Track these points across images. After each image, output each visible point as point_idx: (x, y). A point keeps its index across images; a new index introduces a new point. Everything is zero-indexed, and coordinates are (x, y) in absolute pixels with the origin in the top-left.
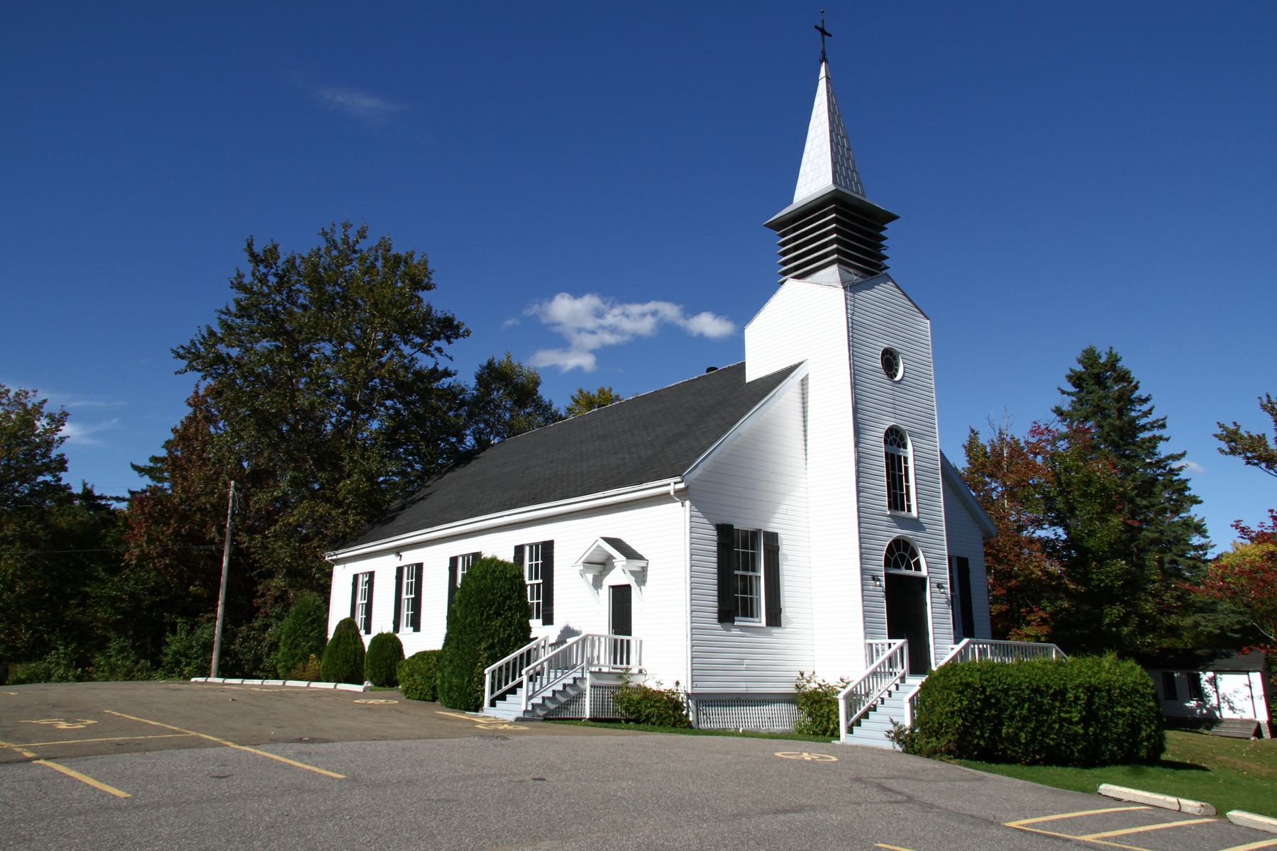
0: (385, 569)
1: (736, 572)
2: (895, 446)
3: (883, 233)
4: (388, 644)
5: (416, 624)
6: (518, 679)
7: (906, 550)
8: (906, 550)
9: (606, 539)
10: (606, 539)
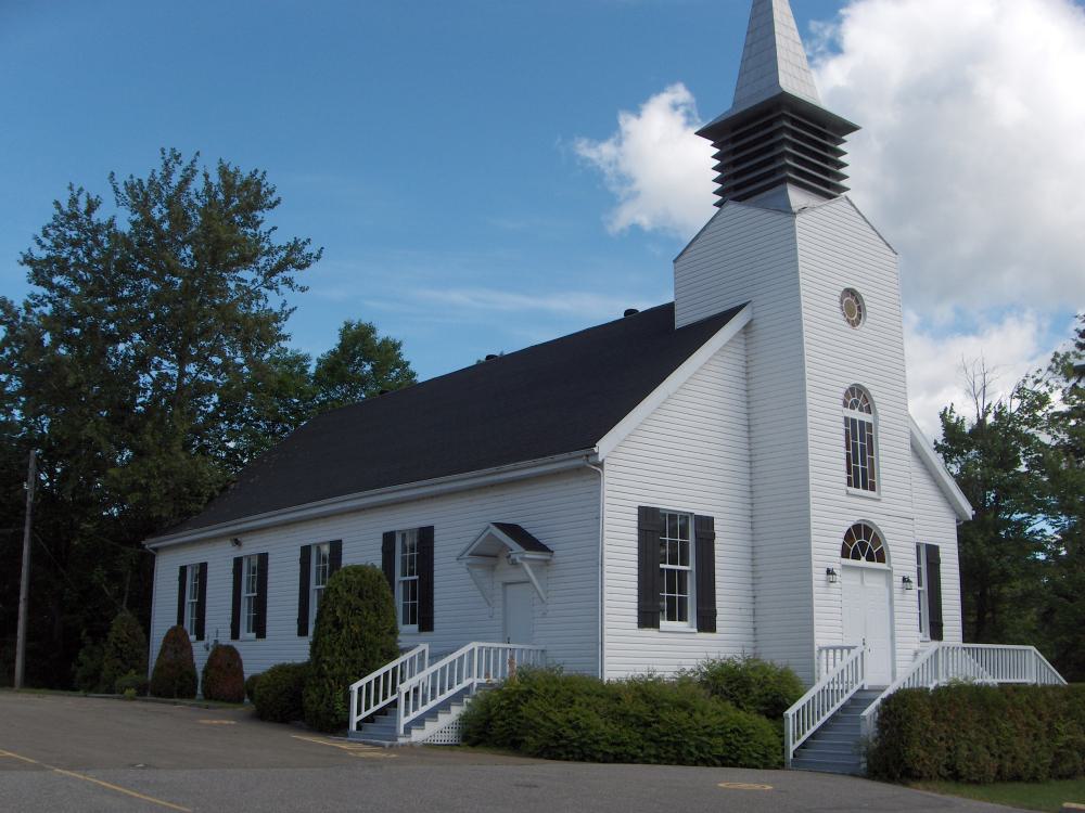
0: (219, 561)
1: (662, 566)
2: (857, 410)
3: (841, 147)
4: (225, 660)
5: (260, 629)
6: (390, 699)
7: (867, 538)
8: (867, 538)
9: (500, 526)
10: (500, 526)
